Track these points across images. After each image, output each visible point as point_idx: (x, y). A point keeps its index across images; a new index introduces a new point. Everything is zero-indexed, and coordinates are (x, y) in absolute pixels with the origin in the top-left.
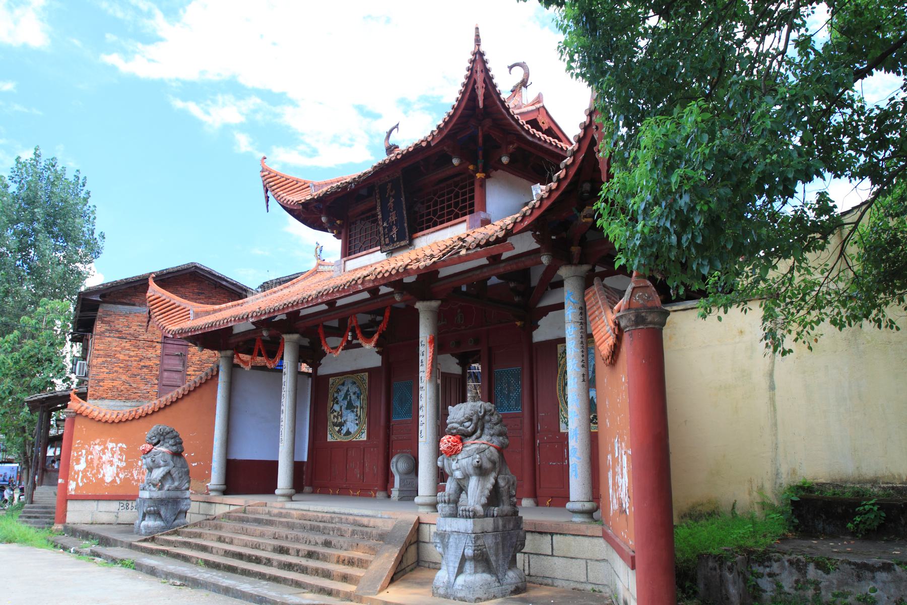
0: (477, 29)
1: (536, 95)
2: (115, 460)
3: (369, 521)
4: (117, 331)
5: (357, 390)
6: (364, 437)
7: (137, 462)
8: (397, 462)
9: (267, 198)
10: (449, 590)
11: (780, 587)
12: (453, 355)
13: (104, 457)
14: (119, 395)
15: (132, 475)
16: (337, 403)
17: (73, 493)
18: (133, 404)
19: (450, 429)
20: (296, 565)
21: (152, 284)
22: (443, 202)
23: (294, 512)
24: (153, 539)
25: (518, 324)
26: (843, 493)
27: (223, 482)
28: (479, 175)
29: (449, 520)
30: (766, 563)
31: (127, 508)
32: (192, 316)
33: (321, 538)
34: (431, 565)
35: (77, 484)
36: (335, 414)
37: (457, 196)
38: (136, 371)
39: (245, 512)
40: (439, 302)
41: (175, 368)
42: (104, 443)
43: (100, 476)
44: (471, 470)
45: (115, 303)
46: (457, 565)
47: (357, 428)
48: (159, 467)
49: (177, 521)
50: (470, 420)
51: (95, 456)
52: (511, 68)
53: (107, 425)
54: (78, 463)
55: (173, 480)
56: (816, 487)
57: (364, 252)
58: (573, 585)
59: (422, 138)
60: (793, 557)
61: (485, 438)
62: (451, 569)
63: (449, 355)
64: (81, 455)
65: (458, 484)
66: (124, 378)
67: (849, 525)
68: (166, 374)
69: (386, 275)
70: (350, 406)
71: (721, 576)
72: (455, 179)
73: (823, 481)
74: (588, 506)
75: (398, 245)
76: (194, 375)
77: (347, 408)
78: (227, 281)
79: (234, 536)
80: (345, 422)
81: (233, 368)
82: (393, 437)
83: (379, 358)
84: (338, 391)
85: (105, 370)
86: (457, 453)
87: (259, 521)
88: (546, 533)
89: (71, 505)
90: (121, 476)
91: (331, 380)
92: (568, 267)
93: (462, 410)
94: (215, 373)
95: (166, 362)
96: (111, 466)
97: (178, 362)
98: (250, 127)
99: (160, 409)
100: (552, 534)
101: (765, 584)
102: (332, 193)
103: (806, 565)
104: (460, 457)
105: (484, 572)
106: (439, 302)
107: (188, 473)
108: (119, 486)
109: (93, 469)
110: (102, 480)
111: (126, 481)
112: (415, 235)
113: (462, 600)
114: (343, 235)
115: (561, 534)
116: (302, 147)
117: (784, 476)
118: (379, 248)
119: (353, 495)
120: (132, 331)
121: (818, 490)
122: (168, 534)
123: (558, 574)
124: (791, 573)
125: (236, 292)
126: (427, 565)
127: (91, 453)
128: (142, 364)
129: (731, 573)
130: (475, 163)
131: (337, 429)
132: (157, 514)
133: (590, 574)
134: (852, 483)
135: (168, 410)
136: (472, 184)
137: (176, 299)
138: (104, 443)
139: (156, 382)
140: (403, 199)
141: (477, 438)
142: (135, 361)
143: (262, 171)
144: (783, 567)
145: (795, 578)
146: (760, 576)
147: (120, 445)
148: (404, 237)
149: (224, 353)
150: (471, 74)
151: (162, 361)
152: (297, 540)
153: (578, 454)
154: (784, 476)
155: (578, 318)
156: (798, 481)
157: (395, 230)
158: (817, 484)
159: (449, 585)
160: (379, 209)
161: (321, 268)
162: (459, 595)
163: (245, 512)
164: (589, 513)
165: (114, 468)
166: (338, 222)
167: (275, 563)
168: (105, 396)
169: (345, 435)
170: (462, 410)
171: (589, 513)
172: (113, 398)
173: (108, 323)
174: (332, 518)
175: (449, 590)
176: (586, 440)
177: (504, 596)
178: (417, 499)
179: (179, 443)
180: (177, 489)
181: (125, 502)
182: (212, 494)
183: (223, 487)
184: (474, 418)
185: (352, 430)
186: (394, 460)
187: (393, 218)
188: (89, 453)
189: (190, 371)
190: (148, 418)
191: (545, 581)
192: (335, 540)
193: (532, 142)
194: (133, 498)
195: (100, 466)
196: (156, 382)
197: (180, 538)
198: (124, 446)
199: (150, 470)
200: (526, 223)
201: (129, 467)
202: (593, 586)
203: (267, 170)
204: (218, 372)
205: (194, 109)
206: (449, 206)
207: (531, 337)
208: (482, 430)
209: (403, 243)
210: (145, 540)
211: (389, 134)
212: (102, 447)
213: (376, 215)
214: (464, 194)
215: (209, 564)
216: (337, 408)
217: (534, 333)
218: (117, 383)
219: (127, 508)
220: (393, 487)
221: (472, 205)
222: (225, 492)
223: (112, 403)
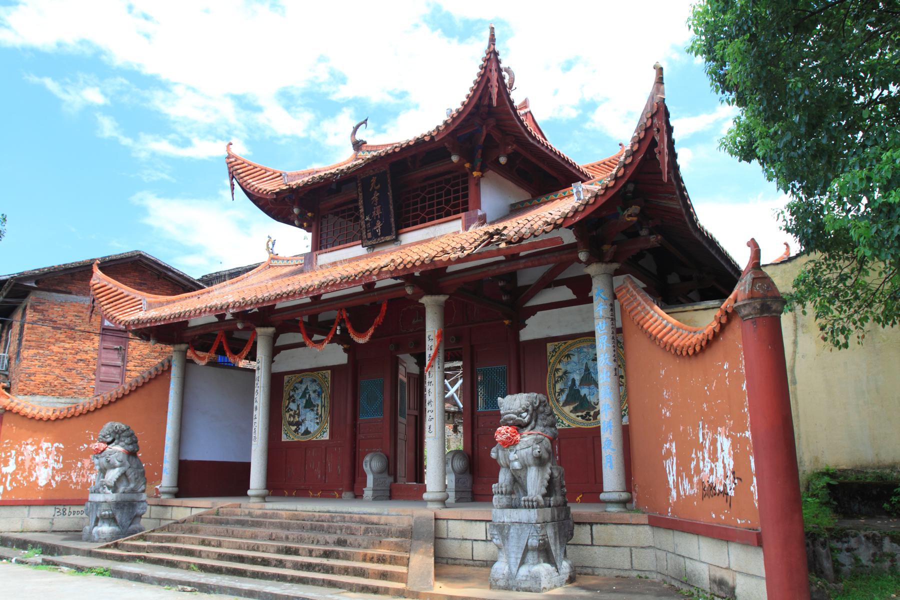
0: (492, 29)
1: (523, 100)
2: (51, 462)
3: (380, 519)
4: (51, 321)
5: (317, 388)
6: (326, 437)
7: (76, 464)
8: (371, 461)
9: (232, 185)
10: (510, 582)
11: (857, 560)
12: (412, 355)
13: (37, 458)
14: (51, 390)
15: (71, 478)
16: (294, 401)
18: (68, 400)
19: (506, 420)
20: (317, 565)
21: (98, 273)
22: (432, 199)
23: (283, 513)
24: (116, 546)
25: (507, 322)
26: (866, 478)
27: (175, 484)
28: (475, 174)
29: (508, 511)
30: (844, 539)
31: (64, 513)
32: (145, 307)
33: (332, 538)
34: (450, 561)
36: (292, 413)
37: (448, 193)
38: (70, 365)
39: (218, 514)
40: (447, 297)
41: (113, 363)
42: (37, 443)
43: (33, 479)
44: (530, 460)
45: (49, 290)
46: (520, 556)
47: (317, 427)
48: (114, 467)
49: (133, 526)
50: (527, 411)
51: (27, 457)
53: (41, 422)
55: (128, 482)
56: (838, 473)
57: (352, 244)
58: (616, 573)
59: (426, 132)
60: (868, 532)
61: (539, 429)
62: (513, 560)
63: (408, 355)
64: (11, 456)
65: (513, 475)
66: (57, 372)
67: (885, 505)
68: (103, 369)
69: (409, 266)
70: (309, 405)
71: (814, 552)
72: (446, 177)
73: (844, 467)
74: (624, 496)
75: (383, 239)
76: (135, 372)
77: (305, 407)
78: (173, 272)
79: (222, 539)
80: (303, 421)
81: (187, 363)
82: (361, 436)
83: (346, 355)
84: (295, 389)
85: (36, 362)
86: (516, 443)
87: (242, 523)
88: (584, 523)
90: (57, 478)
91: (286, 378)
92: (599, 265)
93: (518, 401)
94: (166, 368)
95: (103, 355)
96: (46, 467)
97: (116, 356)
98: (114, 110)
99: (103, 405)
100: (591, 524)
101: (844, 558)
102: (313, 184)
103: (881, 539)
104: (518, 447)
105: (544, 562)
106: (447, 297)
107: (143, 473)
108: (55, 490)
110: (35, 483)
111: (63, 484)
112: (401, 231)
113: (526, 591)
114: (314, 228)
115: (601, 524)
116: (172, 136)
117: (807, 464)
118: (360, 242)
119: (313, 496)
120: (67, 322)
121: (841, 476)
122: (132, 539)
123: (599, 563)
124: (867, 547)
125: (177, 284)
126: (445, 561)
127: (23, 454)
128: (78, 357)
129: (824, 548)
130: (471, 161)
131: (294, 428)
132: (111, 519)
133: (635, 562)
134: (871, 468)
135: (112, 407)
136: (466, 182)
137: (125, 289)
138: (37, 443)
139: (93, 377)
140: (390, 194)
141: (532, 429)
142: (71, 353)
143: (228, 158)
144: (860, 542)
145: (872, 551)
146: (840, 550)
147: (56, 445)
148: (387, 231)
149: (178, 347)
150: (485, 72)
151: (99, 355)
152: (301, 540)
153: (613, 446)
154: (807, 464)
155: (609, 314)
156: (822, 467)
157: (379, 225)
158: (839, 470)
159: (510, 576)
160: (361, 202)
161: (274, 263)
162: (523, 586)
163: (218, 514)
164: (624, 503)
165: (49, 470)
166: (309, 214)
167: (288, 564)
168: (36, 391)
169: (302, 435)
170: (518, 401)
171: (624, 503)
172: (45, 394)
173: (42, 311)
174: (333, 517)
175: (510, 582)
176: (619, 432)
177: (561, 586)
178: (425, 496)
179: (134, 442)
180: (133, 491)
181: (61, 508)
182: (163, 497)
183: (176, 489)
184: (530, 408)
185: (311, 429)
186: (367, 458)
187: (377, 212)
188: (19, 453)
189: (130, 365)
190: (90, 415)
191: (585, 571)
192: (350, 539)
193: (532, 144)
194: (81, 502)
195: (32, 469)
196: (93, 377)
197: (146, 544)
198: (61, 446)
199: (103, 471)
200: (578, 219)
202: (639, 573)
203: (233, 157)
204: (170, 367)
205: (50, 84)
206: (439, 203)
207: (518, 335)
208: (536, 421)
209: (388, 238)
210: (107, 547)
212: (35, 447)
213: (357, 209)
214: (457, 191)
215: (203, 568)
216: (293, 406)
217: (522, 332)
218: (50, 378)
219: (64, 513)
220: (365, 486)
221: (466, 203)
222: (177, 495)
223: (45, 399)
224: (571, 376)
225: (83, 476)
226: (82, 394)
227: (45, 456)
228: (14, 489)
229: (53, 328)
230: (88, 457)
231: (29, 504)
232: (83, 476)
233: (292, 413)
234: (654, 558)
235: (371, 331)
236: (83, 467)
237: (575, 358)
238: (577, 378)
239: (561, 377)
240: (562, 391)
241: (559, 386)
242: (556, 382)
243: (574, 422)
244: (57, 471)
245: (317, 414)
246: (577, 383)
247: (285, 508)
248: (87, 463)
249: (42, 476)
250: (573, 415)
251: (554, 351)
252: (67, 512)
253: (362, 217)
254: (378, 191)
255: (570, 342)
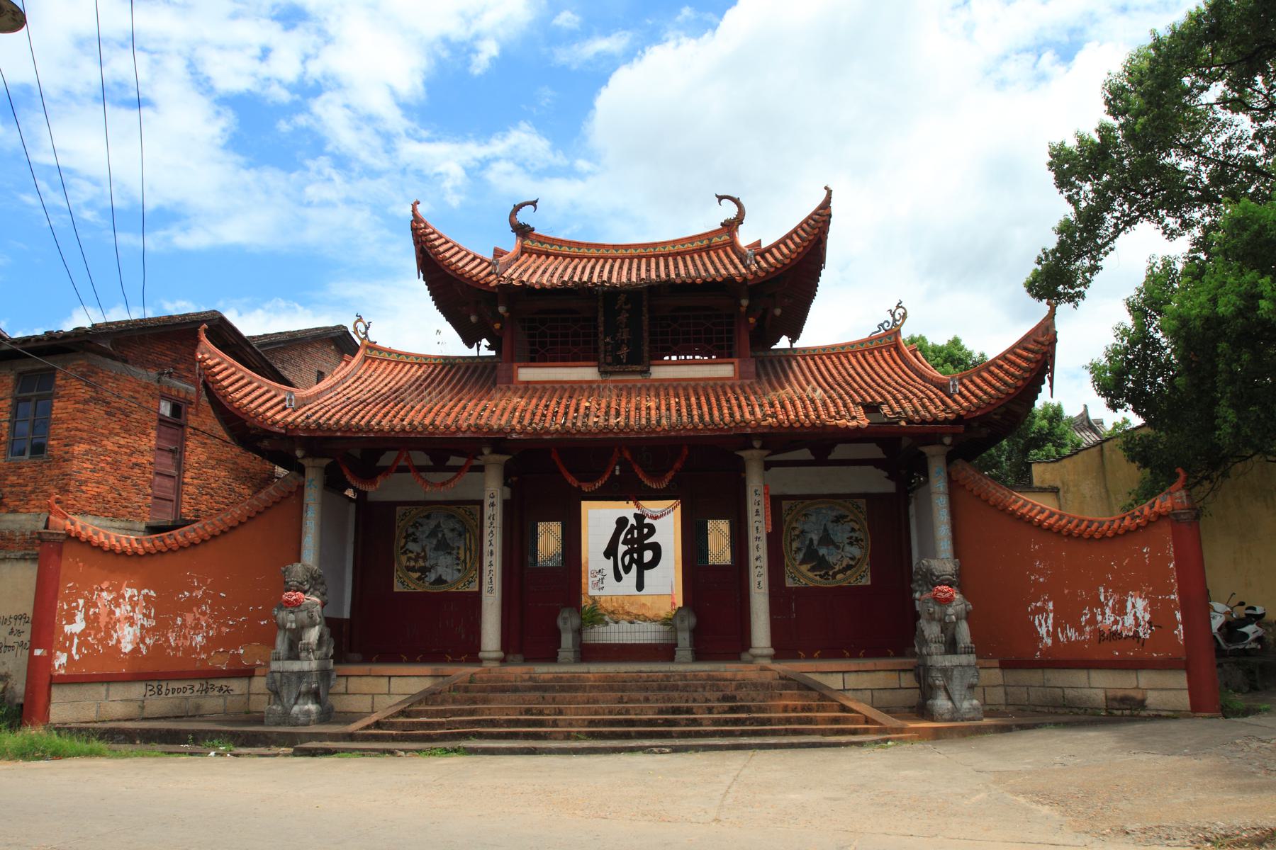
2: (138, 616)
4: (104, 401)
13: (118, 611)
15: (167, 640)
16: (415, 540)
17: (63, 672)
35: (70, 657)
38: (125, 471)
42: (117, 589)
44: (964, 614)
51: (102, 609)
52: (721, 198)
54: (71, 621)
77: (436, 549)
80: (432, 567)
89: (56, 693)
90: (147, 641)
96: (131, 625)
97: (170, 462)
109: (98, 630)
110: (117, 648)
111: (157, 649)
127: (96, 606)
128: (134, 460)
131: (417, 575)
138: (117, 589)
139: (150, 491)
147: (145, 591)
157: (625, 350)
165: (137, 629)
181: (155, 684)
188: (90, 604)
195: (112, 626)
196: (150, 491)
198: (152, 593)
201: (162, 626)
211: (517, 208)
213: (596, 327)
218: (103, 489)
221: (730, 347)
224: (809, 536)
225: (185, 638)
226: (138, 515)
227: (129, 608)
228: (84, 658)
229: (107, 413)
230: (191, 611)
231: (108, 679)
232: (185, 638)
233: (413, 555)
234: (1003, 694)
235: (669, 476)
236: (184, 625)
237: (813, 518)
238: (815, 538)
239: (798, 536)
240: (799, 549)
241: (795, 545)
242: (792, 540)
243: (812, 580)
244: (148, 630)
245: (458, 558)
246: (815, 543)
247: (518, 671)
248: (190, 618)
249: (127, 638)
250: (810, 574)
251: (790, 509)
252: (164, 690)
253: (601, 336)
254: (627, 311)
255: (808, 502)
